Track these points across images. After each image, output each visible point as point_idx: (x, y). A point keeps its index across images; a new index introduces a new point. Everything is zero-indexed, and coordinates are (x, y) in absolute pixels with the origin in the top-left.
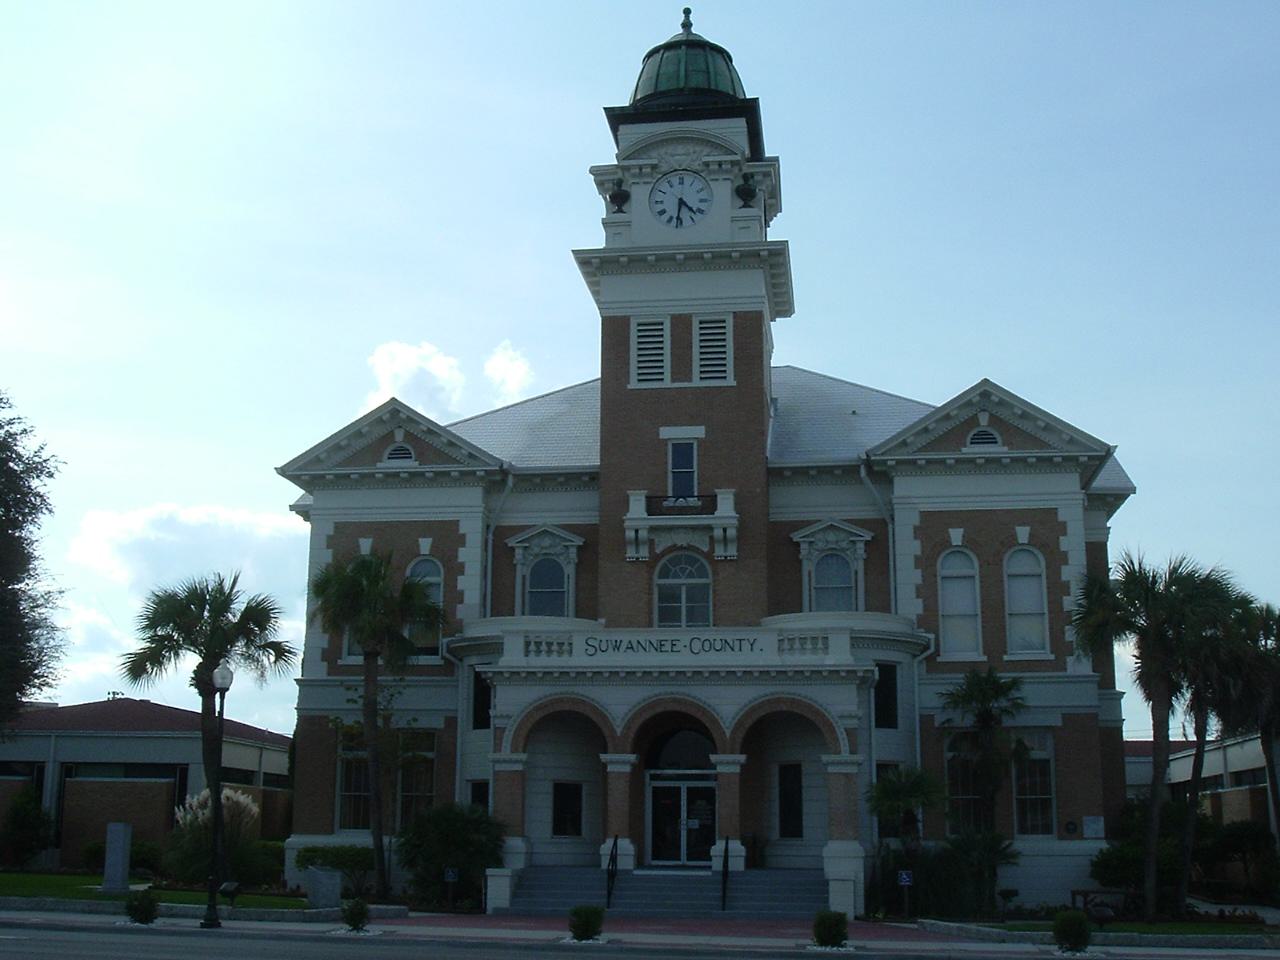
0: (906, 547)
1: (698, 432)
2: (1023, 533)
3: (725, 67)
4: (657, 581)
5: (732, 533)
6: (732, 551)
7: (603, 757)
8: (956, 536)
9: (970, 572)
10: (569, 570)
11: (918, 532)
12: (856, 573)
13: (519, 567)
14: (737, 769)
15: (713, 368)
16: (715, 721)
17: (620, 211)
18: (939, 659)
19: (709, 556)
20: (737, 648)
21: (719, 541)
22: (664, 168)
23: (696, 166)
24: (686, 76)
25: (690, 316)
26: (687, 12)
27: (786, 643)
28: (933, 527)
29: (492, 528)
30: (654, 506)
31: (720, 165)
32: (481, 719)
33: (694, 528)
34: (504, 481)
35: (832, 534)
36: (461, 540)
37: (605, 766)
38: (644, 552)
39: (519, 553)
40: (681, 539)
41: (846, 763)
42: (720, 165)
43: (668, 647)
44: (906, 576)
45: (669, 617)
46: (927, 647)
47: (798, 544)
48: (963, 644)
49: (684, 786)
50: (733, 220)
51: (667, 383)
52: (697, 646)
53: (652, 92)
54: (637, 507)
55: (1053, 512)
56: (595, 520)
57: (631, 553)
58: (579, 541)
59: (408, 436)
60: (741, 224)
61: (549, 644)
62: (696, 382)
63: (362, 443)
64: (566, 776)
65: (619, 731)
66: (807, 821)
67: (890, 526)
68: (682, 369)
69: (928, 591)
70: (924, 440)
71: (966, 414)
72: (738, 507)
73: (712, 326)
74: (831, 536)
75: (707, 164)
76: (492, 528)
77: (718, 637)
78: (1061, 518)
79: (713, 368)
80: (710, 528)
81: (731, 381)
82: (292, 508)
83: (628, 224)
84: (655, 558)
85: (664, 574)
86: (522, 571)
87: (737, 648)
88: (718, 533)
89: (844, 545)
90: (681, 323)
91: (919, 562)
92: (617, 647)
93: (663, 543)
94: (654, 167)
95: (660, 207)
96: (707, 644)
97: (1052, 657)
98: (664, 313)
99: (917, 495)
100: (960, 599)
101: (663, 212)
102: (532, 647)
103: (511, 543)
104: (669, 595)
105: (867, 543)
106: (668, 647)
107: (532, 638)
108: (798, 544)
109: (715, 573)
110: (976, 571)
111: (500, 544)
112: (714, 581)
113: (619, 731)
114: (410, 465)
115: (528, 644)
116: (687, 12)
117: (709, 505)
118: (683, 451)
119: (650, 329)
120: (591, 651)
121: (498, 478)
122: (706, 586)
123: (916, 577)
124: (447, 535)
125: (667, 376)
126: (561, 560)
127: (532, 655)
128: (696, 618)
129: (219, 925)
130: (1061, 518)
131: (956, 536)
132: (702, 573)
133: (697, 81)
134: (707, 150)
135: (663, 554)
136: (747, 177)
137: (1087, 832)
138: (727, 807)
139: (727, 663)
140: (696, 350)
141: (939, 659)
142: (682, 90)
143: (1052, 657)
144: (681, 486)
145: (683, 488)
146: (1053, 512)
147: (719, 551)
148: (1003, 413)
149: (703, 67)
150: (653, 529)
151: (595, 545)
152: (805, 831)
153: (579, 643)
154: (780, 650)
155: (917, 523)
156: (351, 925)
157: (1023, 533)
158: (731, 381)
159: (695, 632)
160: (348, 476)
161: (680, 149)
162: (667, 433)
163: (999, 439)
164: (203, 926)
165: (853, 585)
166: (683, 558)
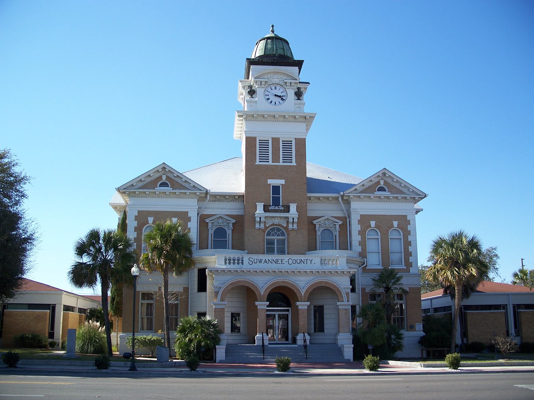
0: (355, 227)
1: (282, 182)
2: (395, 224)
3: (287, 46)
4: (266, 237)
5: (296, 220)
6: (295, 226)
7: (338, 303)
8: (373, 223)
9: (377, 237)
10: (229, 232)
11: (136, 218)
12: (336, 236)
13: (210, 230)
14: (306, 307)
15: (287, 158)
16: (298, 290)
17: (299, 99)
18: (367, 268)
19: (286, 228)
20: (305, 263)
21: (257, 222)
22: (270, 83)
23: (281, 83)
24: (276, 50)
25: (256, 138)
26: (273, 26)
27: (228, 261)
28: (365, 220)
29: (200, 215)
30: (266, 209)
31: (291, 83)
32: (202, 287)
33: (281, 217)
34: (206, 197)
35: (220, 220)
36: (189, 219)
37: (298, 306)
38: (262, 226)
39: (210, 225)
40: (276, 221)
41: (346, 305)
42: (291, 83)
43: (280, 262)
44: (356, 238)
45: (270, 251)
46: (364, 263)
47: (315, 225)
48: (374, 261)
49: (277, 314)
50: (295, 104)
51: (270, 163)
52: (290, 261)
53: (263, 54)
54: (260, 207)
55: (405, 216)
56: (242, 213)
57: (257, 226)
58: (234, 221)
59: (168, 177)
60: (298, 106)
61: (234, 260)
62: (281, 163)
63: (150, 179)
64: (235, 311)
65: (262, 293)
66: (326, 326)
67: (348, 220)
68: (276, 159)
69: (363, 243)
70: (141, 184)
71: (158, 175)
72: (297, 210)
73: (287, 144)
74: (220, 221)
75: (286, 83)
76: (200, 215)
77: (299, 259)
78: (408, 219)
79: (287, 158)
80: (288, 218)
81: (294, 164)
82: (110, 204)
83: (256, 102)
84: (266, 228)
85: (269, 234)
86: (211, 232)
87: (305, 263)
88: (291, 220)
89: (331, 225)
90: (276, 140)
91: (360, 233)
92: (260, 262)
93: (269, 223)
94: (266, 82)
95: (267, 97)
96: (294, 261)
97: (405, 267)
98: (292, 138)
99: (360, 208)
100: (373, 246)
101: (268, 99)
102: (228, 262)
103: (207, 221)
104: (270, 243)
105: (233, 224)
106: (280, 262)
107: (228, 258)
108: (315, 225)
109: (288, 235)
110: (379, 237)
111: (203, 220)
112: (288, 238)
113: (262, 293)
114: (387, 194)
115: (226, 260)
116: (273, 26)
117: (287, 209)
118: (276, 189)
119: (264, 144)
120: (251, 263)
121: (204, 196)
122: (284, 240)
123: (359, 238)
124: (184, 216)
125: (281, 160)
126: (226, 228)
127: (228, 264)
128: (282, 252)
129: (136, 370)
130: (408, 219)
131: (373, 223)
132: (283, 234)
133: (280, 52)
134: (285, 78)
135: (268, 227)
136: (299, 89)
137: (417, 329)
138: (303, 321)
139: (303, 270)
140: (281, 151)
141: (367, 268)
142: (275, 55)
143: (405, 267)
144: (276, 201)
145: (276, 201)
146: (405, 216)
147: (290, 226)
148: (389, 180)
149: (282, 47)
150: (266, 217)
151: (240, 223)
152: (325, 330)
153: (246, 260)
154: (226, 263)
155: (359, 219)
156: (7, 364)
157: (395, 224)
158: (294, 164)
159: (289, 256)
160: (145, 192)
161: (275, 76)
162: (270, 181)
163: (387, 189)
164: (129, 370)
165: (334, 240)
166: (276, 229)
